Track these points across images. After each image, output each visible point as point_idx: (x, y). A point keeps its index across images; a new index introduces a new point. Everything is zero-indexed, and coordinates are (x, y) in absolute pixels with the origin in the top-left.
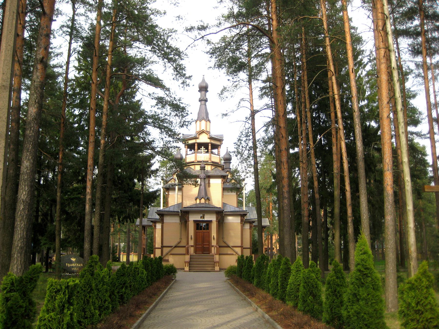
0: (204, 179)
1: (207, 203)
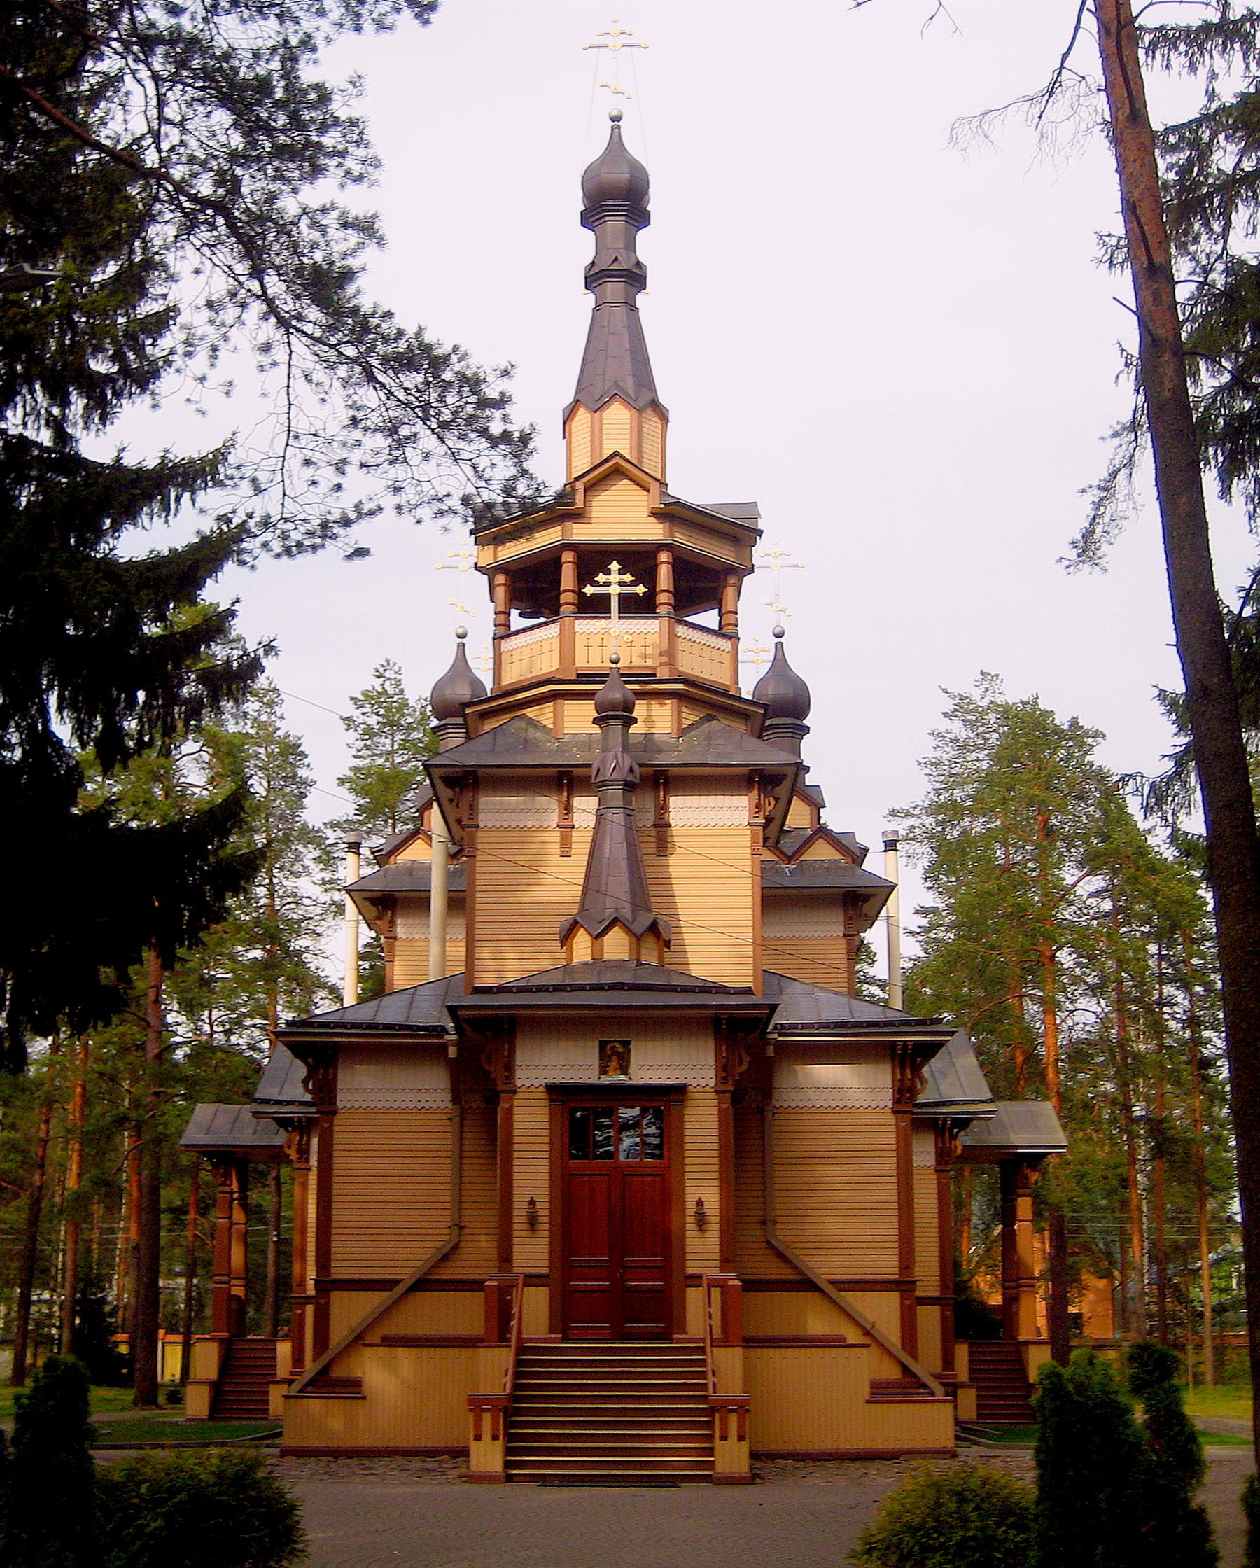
0: (629, 787)
1: (649, 956)
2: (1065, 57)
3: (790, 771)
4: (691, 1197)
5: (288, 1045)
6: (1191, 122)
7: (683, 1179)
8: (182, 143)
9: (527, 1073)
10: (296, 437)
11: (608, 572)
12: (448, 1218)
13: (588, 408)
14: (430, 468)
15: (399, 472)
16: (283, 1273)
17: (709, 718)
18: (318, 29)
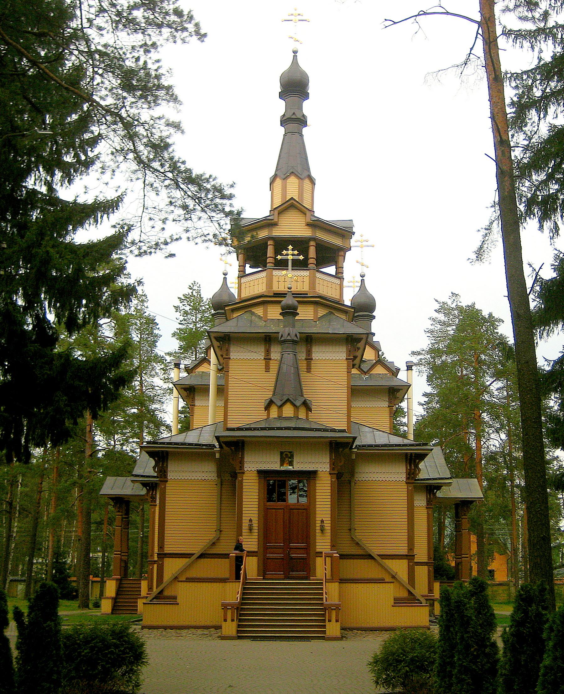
2: (471, 49)
3: (364, 337)
4: (318, 519)
5: (147, 452)
6: (533, 69)
7: (315, 511)
8: (102, 82)
9: (249, 465)
10: (147, 209)
11: (287, 250)
12: (215, 527)
13: (280, 178)
14: (200, 224)
15: (189, 224)
16: (144, 551)
17: (331, 313)
18: (159, 40)
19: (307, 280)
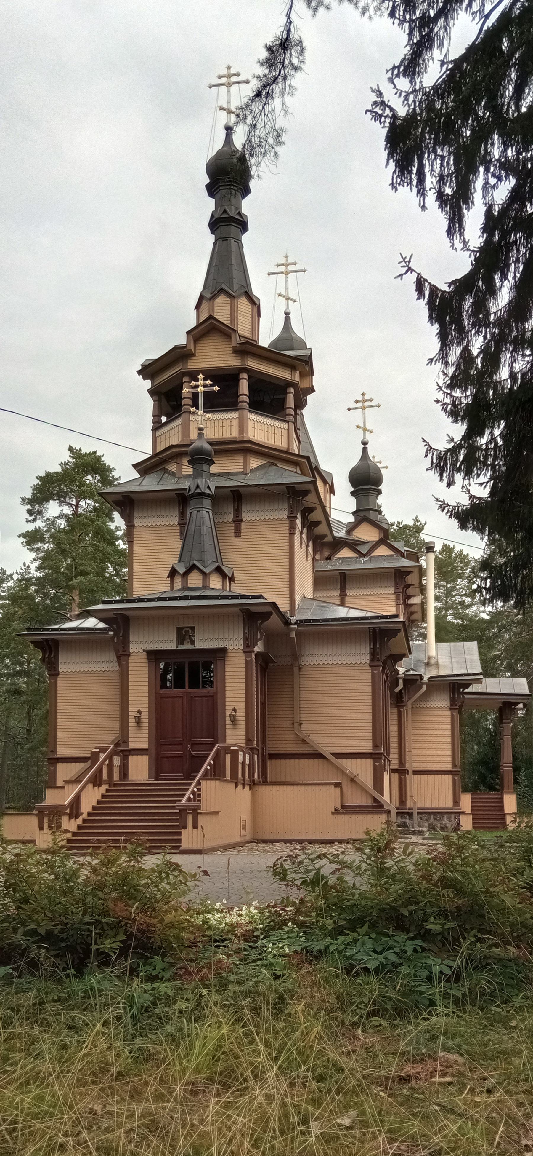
17: (273, 464)
19: (235, 423)
